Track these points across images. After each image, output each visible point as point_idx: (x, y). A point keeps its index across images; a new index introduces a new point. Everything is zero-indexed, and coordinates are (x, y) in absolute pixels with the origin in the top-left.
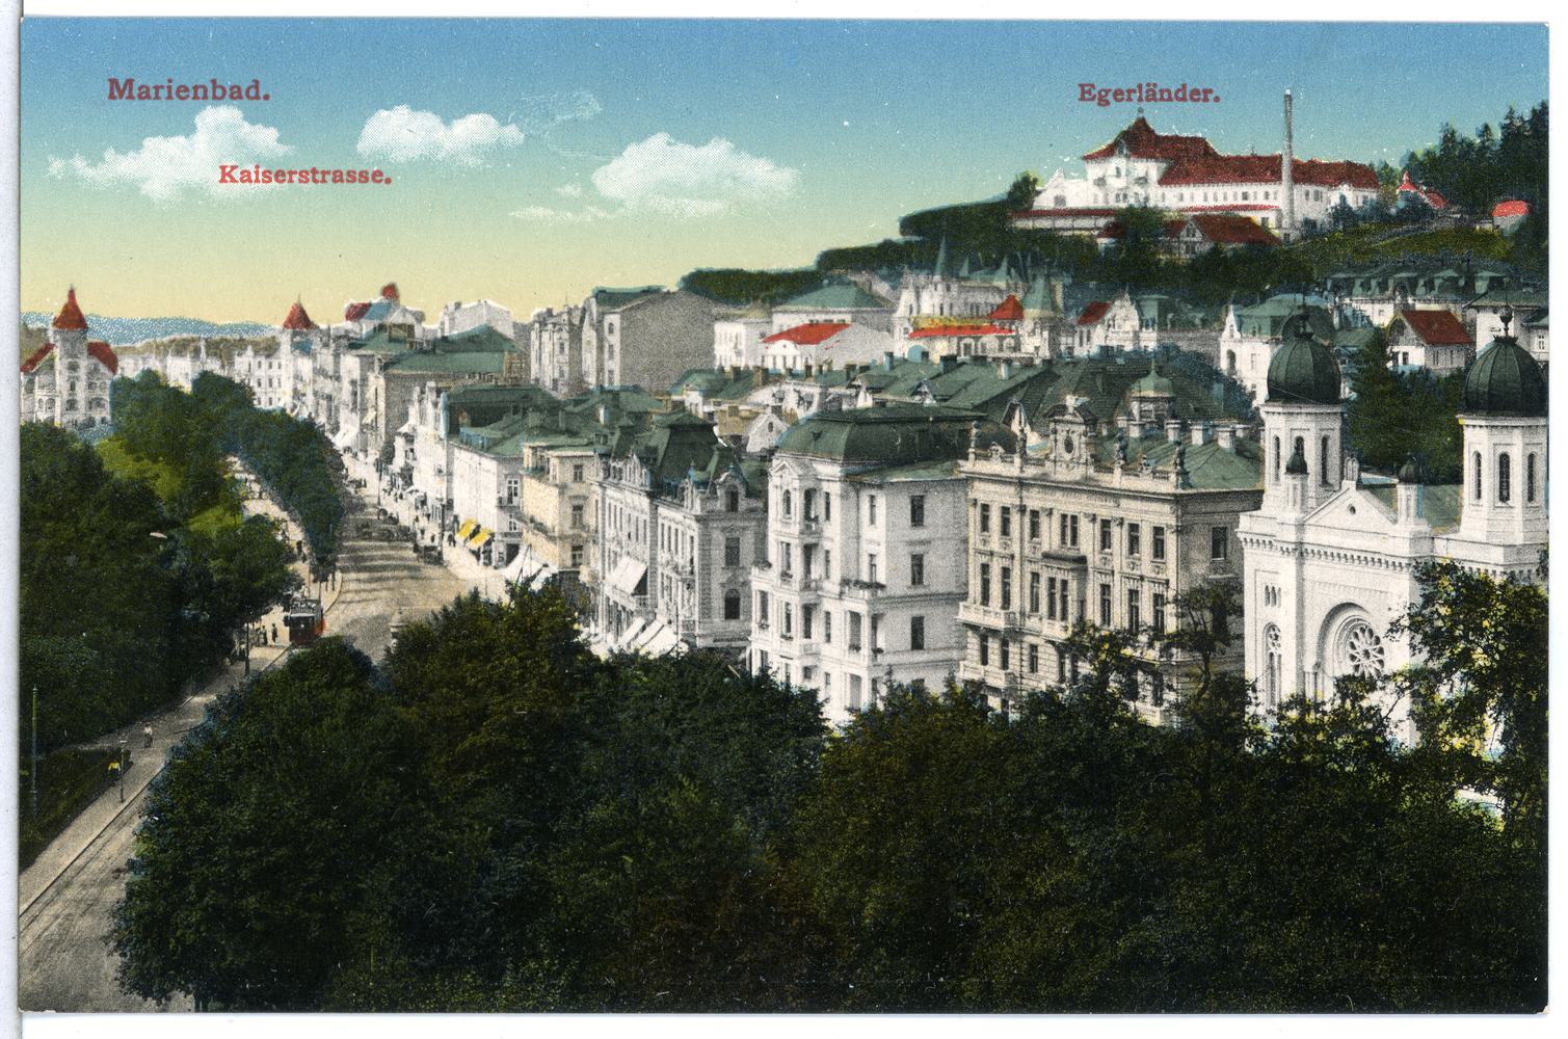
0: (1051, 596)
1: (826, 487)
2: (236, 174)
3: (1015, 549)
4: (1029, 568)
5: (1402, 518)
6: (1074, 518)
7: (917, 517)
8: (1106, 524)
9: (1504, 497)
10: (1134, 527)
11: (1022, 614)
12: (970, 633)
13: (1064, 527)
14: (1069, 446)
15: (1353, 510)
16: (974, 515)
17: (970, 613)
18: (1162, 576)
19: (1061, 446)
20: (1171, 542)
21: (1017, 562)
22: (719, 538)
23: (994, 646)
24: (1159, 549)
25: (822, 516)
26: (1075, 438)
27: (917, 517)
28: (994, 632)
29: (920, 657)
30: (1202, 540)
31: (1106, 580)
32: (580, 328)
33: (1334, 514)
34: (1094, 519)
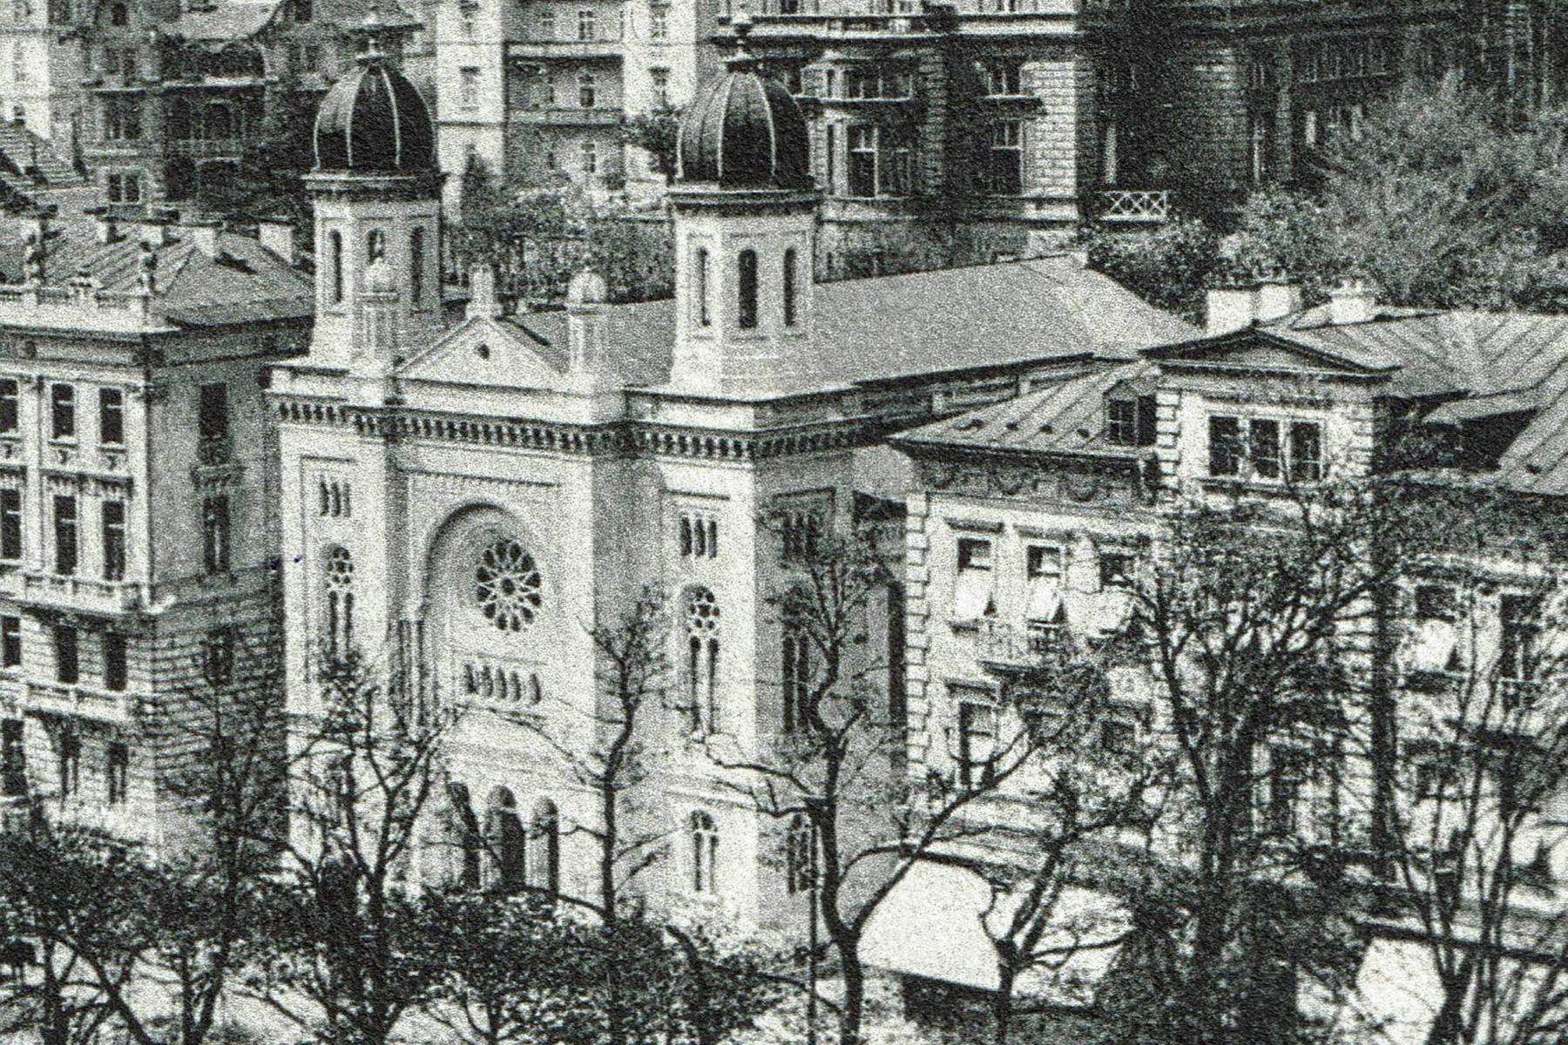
5: (577, 366)
9: (748, 319)
10: (63, 392)
15: (484, 352)
20: (133, 412)
23: (90, 650)
24: (112, 427)
30: (185, 406)
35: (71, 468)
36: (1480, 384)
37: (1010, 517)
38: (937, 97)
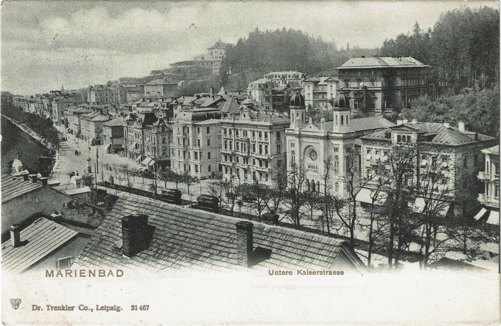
0: (242, 147)
1: (188, 126)
2: (302, 272)
3: (269, 141)
4: (236, 141)
5: (322, 129)
6: (246, 131)
7: (208, 132)
8: (254, 131)
9: (342, 124)
11: (235, 151)
12: (222, 155)
13: (244, 133)
14: (245, 116)
15: (311, 127)
16: (223, 131)
17: (223, 150)
18: (267, 142)
19: (243, 116)
20: (269, 134)
21: (234, 141)
22: (161, 138)
23: (228, 157)
25: (187, 132)
26: (246, 114)
27: (208, 132)
28: (228, 154)
29: (209, 160)
31: (231, 141)
32: (51, 273)
33: (307, 128)
34: (251, 131)
35: (261, 141)
36: (430, 131)
37: (374, 147)
38: (365, 97)
